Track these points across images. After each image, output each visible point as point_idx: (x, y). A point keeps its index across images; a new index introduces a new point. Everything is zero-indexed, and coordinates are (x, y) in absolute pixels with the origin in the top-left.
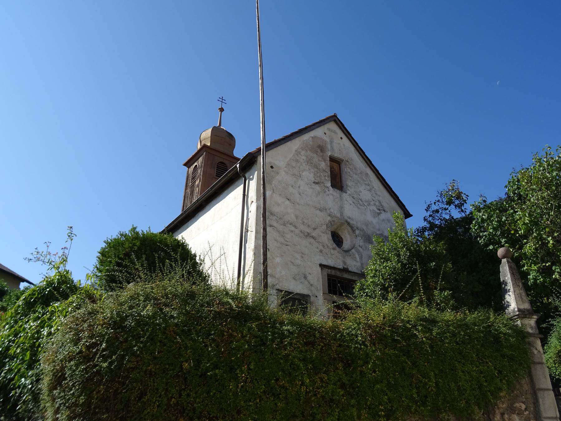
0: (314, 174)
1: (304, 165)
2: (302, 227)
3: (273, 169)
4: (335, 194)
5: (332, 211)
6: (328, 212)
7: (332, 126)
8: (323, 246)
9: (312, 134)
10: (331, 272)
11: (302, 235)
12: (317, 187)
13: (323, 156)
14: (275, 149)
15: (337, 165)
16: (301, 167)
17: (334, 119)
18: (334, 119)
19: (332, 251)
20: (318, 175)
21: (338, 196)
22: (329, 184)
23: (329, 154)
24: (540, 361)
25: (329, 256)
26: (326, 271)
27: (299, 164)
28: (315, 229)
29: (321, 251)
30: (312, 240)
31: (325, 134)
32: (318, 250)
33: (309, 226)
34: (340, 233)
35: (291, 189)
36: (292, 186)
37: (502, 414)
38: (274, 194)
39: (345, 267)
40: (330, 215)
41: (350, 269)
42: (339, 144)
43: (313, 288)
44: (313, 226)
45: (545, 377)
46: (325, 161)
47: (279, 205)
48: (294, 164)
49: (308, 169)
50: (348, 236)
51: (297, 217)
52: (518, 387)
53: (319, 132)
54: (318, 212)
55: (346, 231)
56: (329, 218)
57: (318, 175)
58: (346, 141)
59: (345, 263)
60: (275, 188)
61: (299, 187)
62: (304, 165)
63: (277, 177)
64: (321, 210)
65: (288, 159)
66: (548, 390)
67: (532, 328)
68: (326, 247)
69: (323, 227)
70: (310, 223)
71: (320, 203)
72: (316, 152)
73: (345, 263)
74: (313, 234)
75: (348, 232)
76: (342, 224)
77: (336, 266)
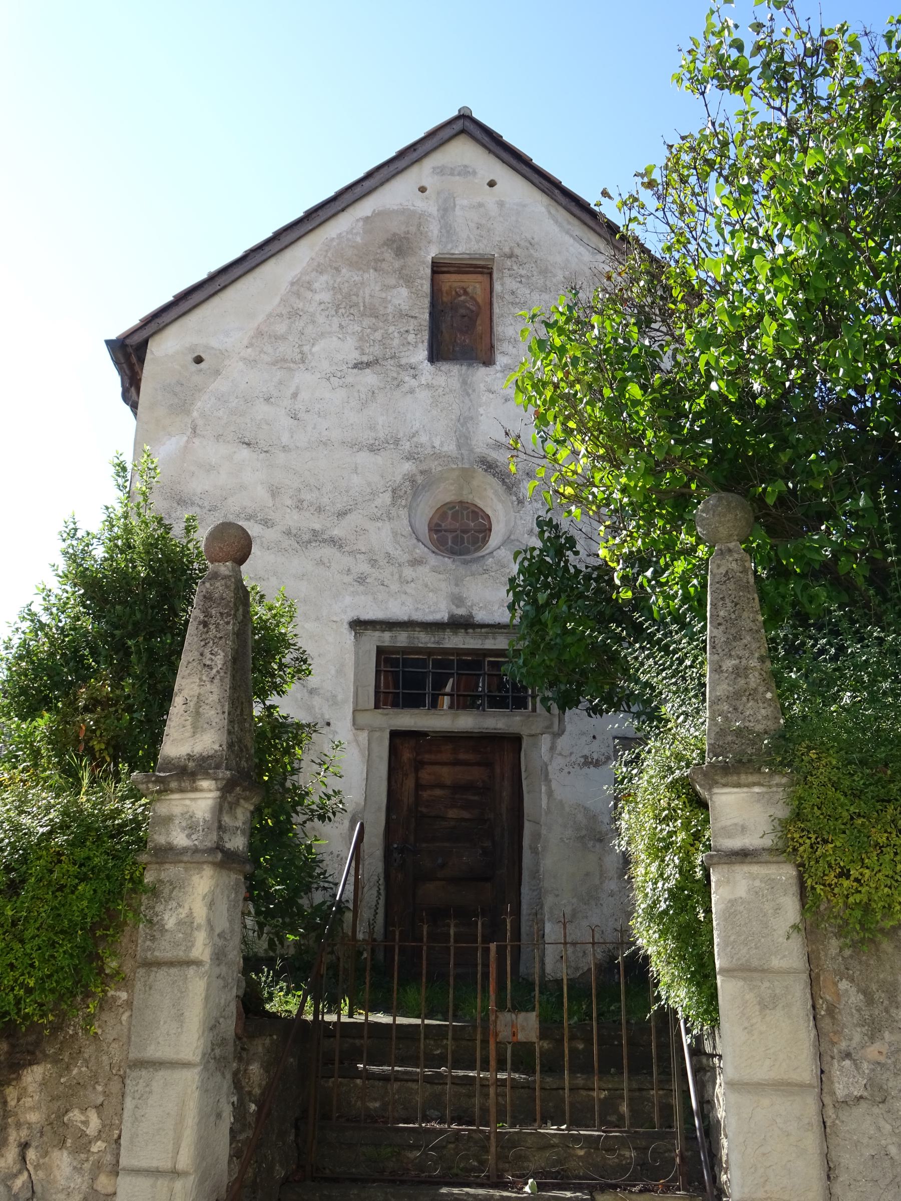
0: (361, 339)
1: (321, 319)
2: (293, 519)
3: (202, 365)
4: (441, 380)
5: (423, 439)
6: (406, 446)
7: (462, 152)
8: (373, 562)
9: (366, 208)
10: (393, 638)
11: (287, 542)
12: (369, 378)
13: (402, 268)
14: (216, 301)
15: (479, 277)
16: (310, 329)
17: (465, 126)
18: (465, 126)
19: (408, 572)
20: (378, 335)
21: (455, 383)
22: (422, 353)
23: (433, 252)
24: (181, 954)
25: (394, 587)
26: (374, 639)
27: (299, 324)
28: (342, 514)
29: (361, 580)
30: (327, 551)
31: (422, 190)
32: (348, 579)
33: (320, 510)
34: (481, 504)
35: (262, 410)
36: (267, 400)
37: (24, 1146)
38: (197, 441)
39: (461, 611)
40: (410, 457)
41: (481, 616)
42: (481, 205)
43: (317, 701)
44: (339, 506)
45: (180, 1017)
46: (408, 281)
47: (210, 468)
48: (281, 328)
49: (335, 327)
50: (499, 507)
51: (275, 492)
52: (88, 1052)
53: (396, 195)
54: (364, 458)
55: (490, 493)
56: (408, 467)
57: (378, 335)
58: (514, 188)
59: (458, 600)
60: (200, 422)
61: (295, 395)
62: (321, 319)
63: (212, 387)
64: (373, 449)
65: (261, 318)
66: (186, 1065)
67: (191, 828)
68: (382, 562)
69: (378, 502)
70: (325, 500)
71: (372, 428)
72: (377, 265)
73: (458, 600)
74: (336, 532)
75: (496, 493)
76: (466, 475)
77: (418, 616)
